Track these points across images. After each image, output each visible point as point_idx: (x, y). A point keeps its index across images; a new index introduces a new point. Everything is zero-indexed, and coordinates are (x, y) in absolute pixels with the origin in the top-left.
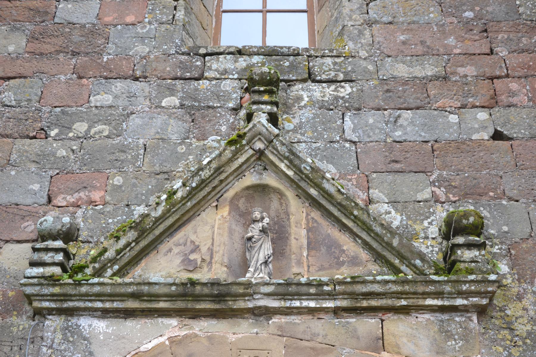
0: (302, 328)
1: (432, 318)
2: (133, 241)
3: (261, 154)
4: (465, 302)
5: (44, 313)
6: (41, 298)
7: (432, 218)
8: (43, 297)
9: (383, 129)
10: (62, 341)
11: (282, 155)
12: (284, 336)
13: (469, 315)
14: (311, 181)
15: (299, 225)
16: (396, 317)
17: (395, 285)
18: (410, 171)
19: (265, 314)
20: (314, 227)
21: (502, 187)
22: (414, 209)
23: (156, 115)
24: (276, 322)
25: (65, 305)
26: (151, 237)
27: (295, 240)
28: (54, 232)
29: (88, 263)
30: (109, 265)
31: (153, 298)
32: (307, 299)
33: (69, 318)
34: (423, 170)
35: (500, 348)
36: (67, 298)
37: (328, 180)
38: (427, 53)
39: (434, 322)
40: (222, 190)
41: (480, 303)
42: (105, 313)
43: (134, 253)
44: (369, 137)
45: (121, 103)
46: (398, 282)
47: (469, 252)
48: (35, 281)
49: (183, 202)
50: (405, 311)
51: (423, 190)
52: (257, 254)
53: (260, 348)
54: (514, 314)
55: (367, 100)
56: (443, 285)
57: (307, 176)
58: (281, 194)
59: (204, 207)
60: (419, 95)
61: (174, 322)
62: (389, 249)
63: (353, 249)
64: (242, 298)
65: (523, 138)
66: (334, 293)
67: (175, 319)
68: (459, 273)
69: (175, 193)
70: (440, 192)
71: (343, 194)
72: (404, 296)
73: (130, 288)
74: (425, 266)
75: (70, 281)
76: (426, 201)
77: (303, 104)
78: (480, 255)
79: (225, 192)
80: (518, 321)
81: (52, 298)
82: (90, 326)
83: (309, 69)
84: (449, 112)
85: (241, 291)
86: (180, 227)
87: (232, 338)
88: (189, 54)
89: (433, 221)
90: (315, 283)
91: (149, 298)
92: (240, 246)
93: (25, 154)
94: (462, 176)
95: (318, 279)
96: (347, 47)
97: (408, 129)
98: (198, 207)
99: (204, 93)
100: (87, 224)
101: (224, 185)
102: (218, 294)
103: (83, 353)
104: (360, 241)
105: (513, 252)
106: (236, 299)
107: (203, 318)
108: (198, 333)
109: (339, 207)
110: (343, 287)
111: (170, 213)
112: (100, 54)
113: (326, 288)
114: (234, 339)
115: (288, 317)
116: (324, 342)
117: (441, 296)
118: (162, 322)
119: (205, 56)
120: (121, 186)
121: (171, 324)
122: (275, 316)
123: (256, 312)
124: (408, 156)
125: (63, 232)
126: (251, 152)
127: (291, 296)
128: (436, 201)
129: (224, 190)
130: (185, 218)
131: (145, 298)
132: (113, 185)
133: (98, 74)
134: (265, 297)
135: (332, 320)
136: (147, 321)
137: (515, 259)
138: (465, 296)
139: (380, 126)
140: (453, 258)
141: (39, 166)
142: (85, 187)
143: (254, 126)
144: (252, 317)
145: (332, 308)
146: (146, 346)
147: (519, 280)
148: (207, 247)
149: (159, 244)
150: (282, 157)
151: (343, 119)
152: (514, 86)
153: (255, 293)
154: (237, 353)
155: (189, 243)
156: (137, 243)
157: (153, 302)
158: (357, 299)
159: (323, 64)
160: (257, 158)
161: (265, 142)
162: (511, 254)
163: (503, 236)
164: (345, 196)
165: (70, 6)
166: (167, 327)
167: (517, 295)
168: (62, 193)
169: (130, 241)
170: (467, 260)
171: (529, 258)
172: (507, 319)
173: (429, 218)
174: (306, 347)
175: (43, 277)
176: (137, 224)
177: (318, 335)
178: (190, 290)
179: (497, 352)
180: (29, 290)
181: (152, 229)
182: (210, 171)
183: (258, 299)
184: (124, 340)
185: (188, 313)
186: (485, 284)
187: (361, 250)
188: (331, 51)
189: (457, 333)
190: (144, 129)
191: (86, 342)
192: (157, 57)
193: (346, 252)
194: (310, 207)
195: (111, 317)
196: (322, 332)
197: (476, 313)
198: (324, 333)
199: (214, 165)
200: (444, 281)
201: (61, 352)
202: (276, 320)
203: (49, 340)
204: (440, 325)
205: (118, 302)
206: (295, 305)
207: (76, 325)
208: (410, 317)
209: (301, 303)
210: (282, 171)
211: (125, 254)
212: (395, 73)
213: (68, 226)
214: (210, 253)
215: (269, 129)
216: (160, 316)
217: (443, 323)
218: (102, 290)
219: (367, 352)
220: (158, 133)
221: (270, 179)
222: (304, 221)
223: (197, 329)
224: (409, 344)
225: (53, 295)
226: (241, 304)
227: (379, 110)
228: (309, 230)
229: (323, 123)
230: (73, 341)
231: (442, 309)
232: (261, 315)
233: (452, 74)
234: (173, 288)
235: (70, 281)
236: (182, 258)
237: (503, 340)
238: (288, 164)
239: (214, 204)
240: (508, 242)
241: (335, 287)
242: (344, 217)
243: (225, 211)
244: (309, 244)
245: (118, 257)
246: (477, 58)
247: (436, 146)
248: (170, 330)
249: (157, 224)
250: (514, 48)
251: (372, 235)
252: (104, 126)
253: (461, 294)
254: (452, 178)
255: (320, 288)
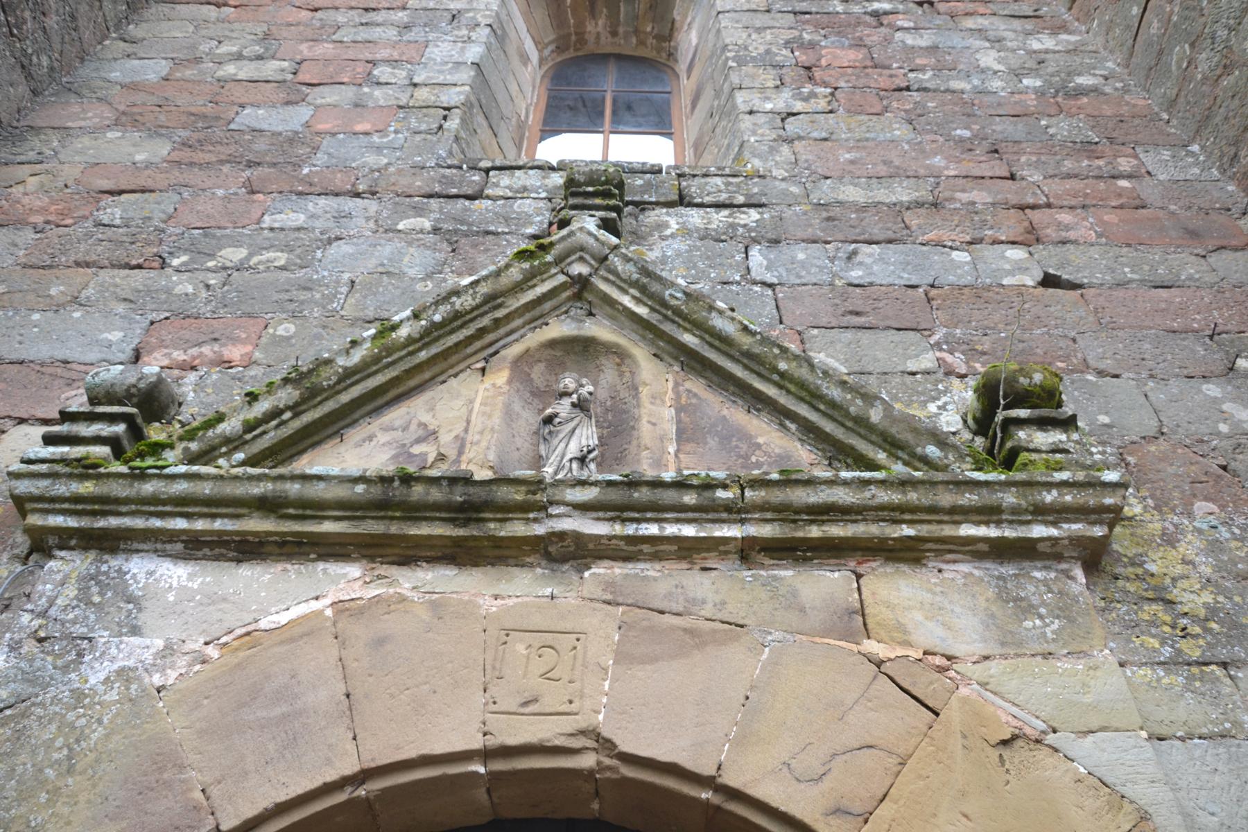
0: (663, 587)
1: (976, 572)
2: (288, 408)
3: (582, 284)
4: (1053, 532)
5: (51, 542)
6: (47, 506)
7: (944, 399)
8: (50, 503)
9: (826, 267)
10: (75, 602)
11: (625, 281)
12: (618, 604)
13: (1064, 566)
14: (685, 319)
15: (658, 401)
16: (890, 569)
17: (885, 490)
18: (888, 328)
19: (574, 558)
20: (691, 404)
21: (1079, 355)
22: (904, 384)
23: (383, 242)
24: (599, 575)
25: (101, 523)
26: (330, 406)
27: (649, 426)
28: (120, 390)
29: (174, 438)
30: (224, 449)
31: (309, 512)
32: (678, 521)
33: (106, 557)
34: (914, 326)
35: (1152, 640)
36: (107, 508)
37: (721, 312)
38: (897, 175)
39: (983, 580)
40: (497, 341)
41: (1088, 534)
42: (194, 548)
43: (286, 431)
44: (800, 277)
45: (319, 224)
46: (892, 484)
47: (1044, 435)
48: (44, 468)
49: (411, 349)
50: (908, 553)
51: (917, 356)
52: (562, 445)
53: (559, 629)
54: (1165, 571)
55: (791, 228)
56: (997, 491)
57: (677, 312)
58: (621, 355)
59: (456, 369)
60: (890, 225)
61: (354, 570)
62: (862, 431)
63: (778, 442)
64: (520, 516)
65: (1102, 285)
66: (740, 504)
67: (357, 565)
68: (1030, 467)
69: (394, 328)
70: (957, 361)
71: (753, 334)
72: (907, 517)
73: (258, 486)
74: (950, 457)
75: (124, 469)
76: (927, 373)
77: (668, 232)
78: (1069, 440)
79: (504, 346)
80: (1179, 584)
81: (73, 507)
82: (151, 573)
83: (680, 190)
84: (951, 248)
85: (519, 497)
86: (398, 399)
87: (493, 606)
88: (461, 168)
89: (946, 403)
90: (695, 482)
91: (300, 512)
92: (527, 445)
93: (111, 289)
94: (994, 337)
95: (703, 474)
96: (749, 166)
97: (875, 268)
98: (443, 365)
99: (481, 214)
100: (202, 395)
101: (502, 331)
102: (465, 502)
103: (117, 628)
104: (793, 427)
105: (1130, 459)
106: (506, 516)
107: (424, 564)
108: (409, 594)
109: (745, 361)
110: (763, 493)
111: (380, 365)
112: (297, 166)
113: (721, 494)
114: (494, 609)
115: (630, 566)
116: (719, 616)
117: (995, 518)
118: (325, 570)
119: (487, 171)
120: (290, 338)
121: (345, 575)
122: (599, 562)
123: (552, 549)
124: (881, 305)
125: (139, 390)
126: (562, 278)
127: (639, 511)
128: (948, 373)
129: (501, 343)
130: (412, 383)
131: (291, 511)
132: (274, 335)
133: (287, 188)
134: (577, 513)
135: (736, 573)
136: (289, 566)
137: (1139, 471)
138: (1051, 518)
139: (819, 263)
140: (1009, 445)
141: (132, 306)
142: (216, 340)
143: (571, 234)
144: (544, 563)
145: (735, 539)
146: (275, 618)
147: (1157, 508)
148: (453, 434)
149: (348, 426)
150: (624, 284)
151: (746, 253)
152: (1065, 217)
153: (551, 503)
154: (498, 639)
155: (413, 427)
156: (296, 415)
157: (308, 522)
158: (794, 521)
159: (706, 184)
160: (574, 294)
161: (593, 262)
162: (1127, 465)
163: (1103, 434)
164: (758, 337)
165: (261, 112)
166: (335, 580)
167: (1164, 534)
168: (166, 347)
169: (281, 406)
170: (1044, 448)
171: (1171, 470)
172: (1153, 582)
173: (938, 399)
174: (673, 628)
175: (63, 461)
176: (303, 376)
177: (704, 602)
178: (397, 493)
179: (1147, 649)
180: (23, 487)
181: (334, 390)
182: (474, 299)
183: (558, 516)
184: (224, 606)
185: (389, 551)
186: (1095, 490)
187: (798, 445)
188: (719, 169)
189: (1043, 603)
190: (357, 259)
191: (131, 606)
192: (400, 171)
193: (764, 448)
194: (682, 373)
195: (205, 558)
196: (711, 597)
197: (1079, 563)
198: (718, 599)
199: (484, 289)
200: (1000, 483)
201: (63, 625)
202: (602, 571)
203: (44, 600)
204: (997, 586)
205: (226, 520)
206: (647, 533)
207: (119, 571)
208: (924, 570)
209: (661, 528)
210: (626, 308)
211: (264, 433)
212: (841, 197)
213: (153, 379)
214: (458, 444)
215: (601, 237)
216: (323, 557)
217: (1005, 582)
218: (191, 490)
219: (826, 641)
220: (382, 265)
221: (600, 329)
222: (670, 394)
223: (407, 585)
224: (930, 625)
225: (77, 499)
226: (517, 529)
227: (815, 242)
228: (680, 409)
229: (708, 258)
230: (100, 603)
231: (1000, 551)
232: (563, 560)
233: (946, 200)
234: (360, 488)
235: (124, 469)
236: (394, 452)
237: (1152, 623)
238: (638, 294)
239: (479, 365)
240: (1118, 443)
241: (743, 493)
242: (757, 379)
243: (500, 377)
244: (680, 433)
245: (248, 436)
246: (988, 182)
247: (933, 292)
248: (341, 586)
249: (348, 382)
250: (1051, 172)
251: (822, 407)
252: (279, 254)
253: (1041, 513)
254: (975, 338)
255: (707, 494)
